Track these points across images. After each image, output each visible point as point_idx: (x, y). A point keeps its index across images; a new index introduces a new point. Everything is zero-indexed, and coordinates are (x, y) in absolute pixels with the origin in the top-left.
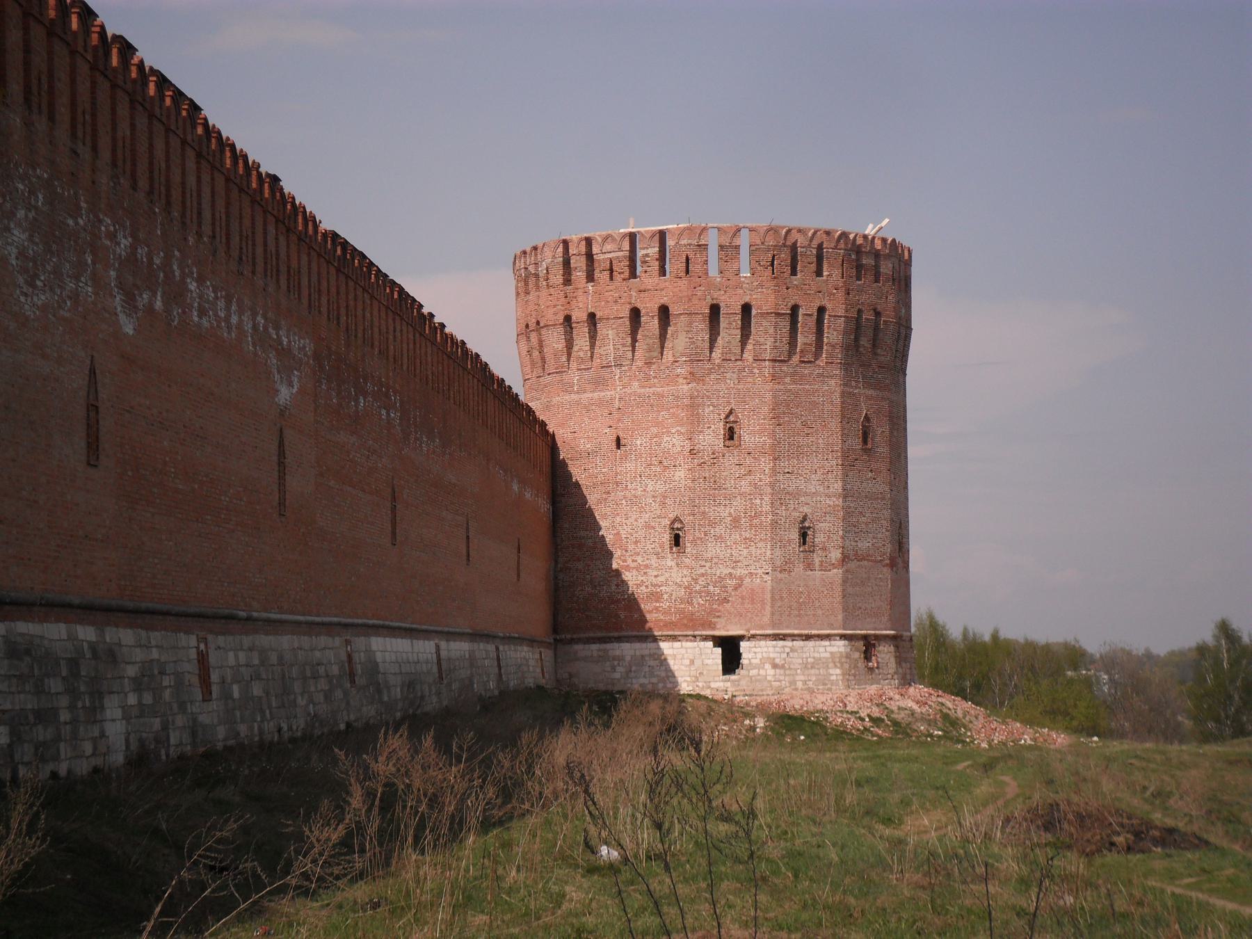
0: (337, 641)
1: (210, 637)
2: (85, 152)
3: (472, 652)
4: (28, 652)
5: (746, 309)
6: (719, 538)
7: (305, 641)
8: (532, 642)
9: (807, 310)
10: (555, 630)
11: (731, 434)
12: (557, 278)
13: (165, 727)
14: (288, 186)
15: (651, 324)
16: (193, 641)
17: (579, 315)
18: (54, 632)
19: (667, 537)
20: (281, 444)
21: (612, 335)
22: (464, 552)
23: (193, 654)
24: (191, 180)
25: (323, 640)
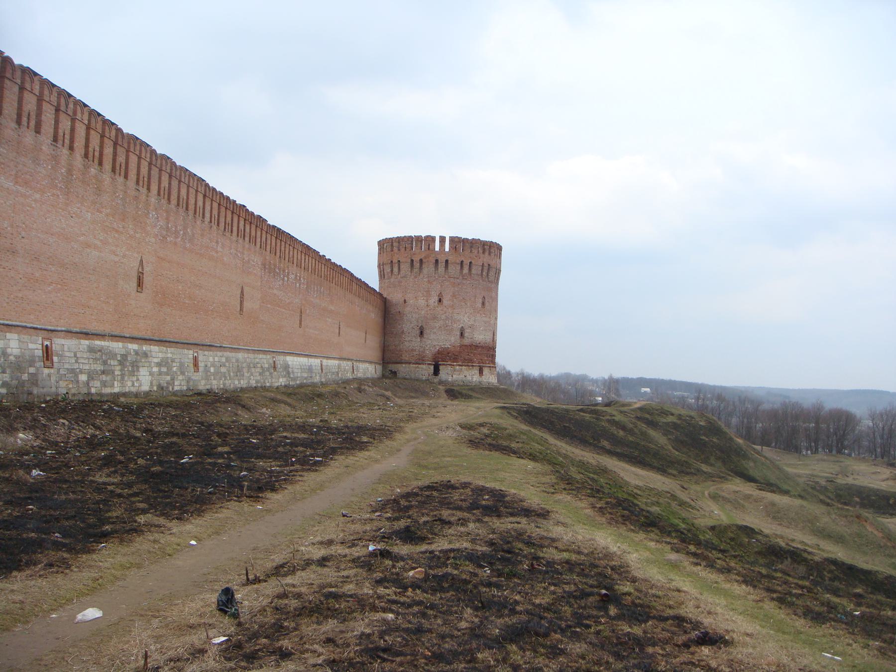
0: (268, 357)
1: (200, 352)
2: (144, 190)
3: (339, 366)
4: (100, 351)
5: (447, 261)
6: (435, 333)
7: (251, 356)
8: (371, 362)
9: (466, 262)
10: (383, 359)
11: (440, 301)
12: (389, 249)
13: (173, 379)
14: (250, 208)
15: (417, 265)
16: (191, 352)
17: (395, 261)
18: (117, 346)
19: (418, 332)
20: (242, 292)
21: (405, 267)
22: (337, 331)
23: (191, 356)
24: (200, 203)
25: (261, 356)
